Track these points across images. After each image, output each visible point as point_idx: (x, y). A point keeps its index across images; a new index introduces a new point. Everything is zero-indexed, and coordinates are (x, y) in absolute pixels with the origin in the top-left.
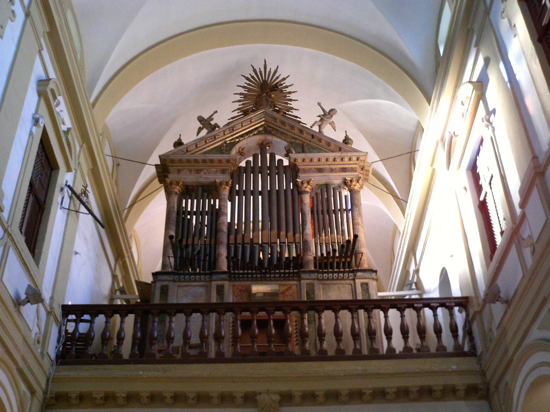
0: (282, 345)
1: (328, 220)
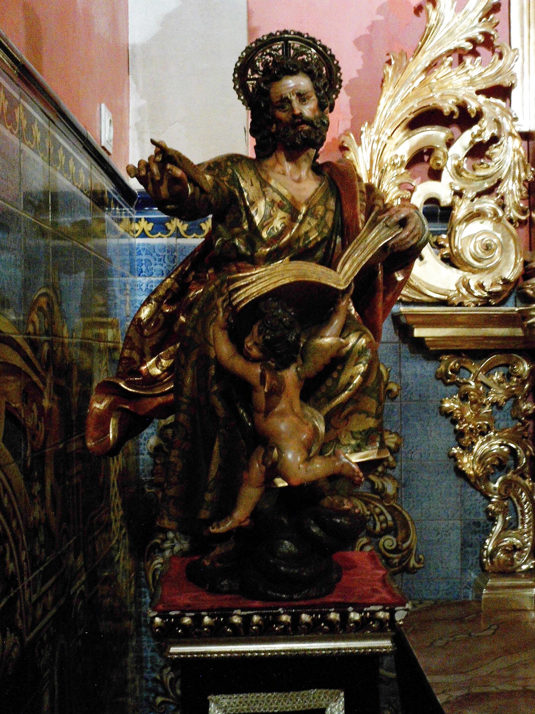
0: (375, 247)
1: (241, 299)
